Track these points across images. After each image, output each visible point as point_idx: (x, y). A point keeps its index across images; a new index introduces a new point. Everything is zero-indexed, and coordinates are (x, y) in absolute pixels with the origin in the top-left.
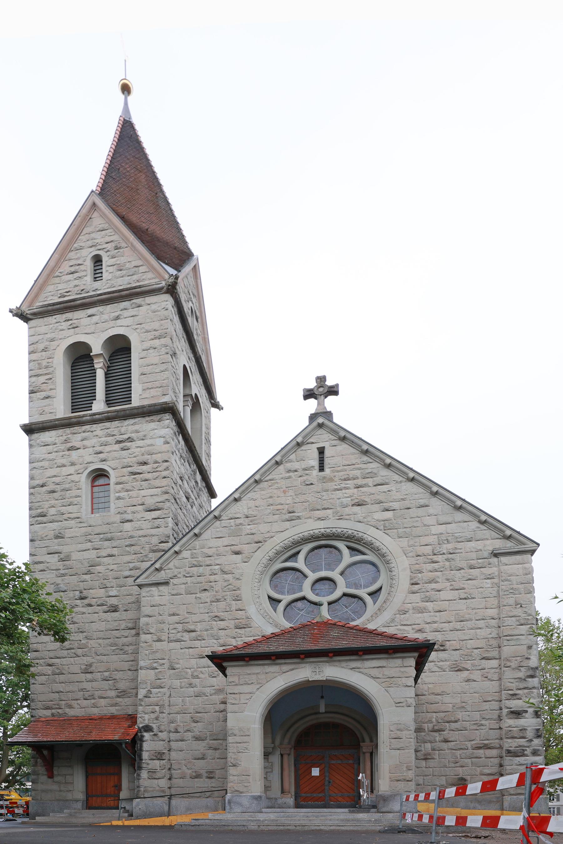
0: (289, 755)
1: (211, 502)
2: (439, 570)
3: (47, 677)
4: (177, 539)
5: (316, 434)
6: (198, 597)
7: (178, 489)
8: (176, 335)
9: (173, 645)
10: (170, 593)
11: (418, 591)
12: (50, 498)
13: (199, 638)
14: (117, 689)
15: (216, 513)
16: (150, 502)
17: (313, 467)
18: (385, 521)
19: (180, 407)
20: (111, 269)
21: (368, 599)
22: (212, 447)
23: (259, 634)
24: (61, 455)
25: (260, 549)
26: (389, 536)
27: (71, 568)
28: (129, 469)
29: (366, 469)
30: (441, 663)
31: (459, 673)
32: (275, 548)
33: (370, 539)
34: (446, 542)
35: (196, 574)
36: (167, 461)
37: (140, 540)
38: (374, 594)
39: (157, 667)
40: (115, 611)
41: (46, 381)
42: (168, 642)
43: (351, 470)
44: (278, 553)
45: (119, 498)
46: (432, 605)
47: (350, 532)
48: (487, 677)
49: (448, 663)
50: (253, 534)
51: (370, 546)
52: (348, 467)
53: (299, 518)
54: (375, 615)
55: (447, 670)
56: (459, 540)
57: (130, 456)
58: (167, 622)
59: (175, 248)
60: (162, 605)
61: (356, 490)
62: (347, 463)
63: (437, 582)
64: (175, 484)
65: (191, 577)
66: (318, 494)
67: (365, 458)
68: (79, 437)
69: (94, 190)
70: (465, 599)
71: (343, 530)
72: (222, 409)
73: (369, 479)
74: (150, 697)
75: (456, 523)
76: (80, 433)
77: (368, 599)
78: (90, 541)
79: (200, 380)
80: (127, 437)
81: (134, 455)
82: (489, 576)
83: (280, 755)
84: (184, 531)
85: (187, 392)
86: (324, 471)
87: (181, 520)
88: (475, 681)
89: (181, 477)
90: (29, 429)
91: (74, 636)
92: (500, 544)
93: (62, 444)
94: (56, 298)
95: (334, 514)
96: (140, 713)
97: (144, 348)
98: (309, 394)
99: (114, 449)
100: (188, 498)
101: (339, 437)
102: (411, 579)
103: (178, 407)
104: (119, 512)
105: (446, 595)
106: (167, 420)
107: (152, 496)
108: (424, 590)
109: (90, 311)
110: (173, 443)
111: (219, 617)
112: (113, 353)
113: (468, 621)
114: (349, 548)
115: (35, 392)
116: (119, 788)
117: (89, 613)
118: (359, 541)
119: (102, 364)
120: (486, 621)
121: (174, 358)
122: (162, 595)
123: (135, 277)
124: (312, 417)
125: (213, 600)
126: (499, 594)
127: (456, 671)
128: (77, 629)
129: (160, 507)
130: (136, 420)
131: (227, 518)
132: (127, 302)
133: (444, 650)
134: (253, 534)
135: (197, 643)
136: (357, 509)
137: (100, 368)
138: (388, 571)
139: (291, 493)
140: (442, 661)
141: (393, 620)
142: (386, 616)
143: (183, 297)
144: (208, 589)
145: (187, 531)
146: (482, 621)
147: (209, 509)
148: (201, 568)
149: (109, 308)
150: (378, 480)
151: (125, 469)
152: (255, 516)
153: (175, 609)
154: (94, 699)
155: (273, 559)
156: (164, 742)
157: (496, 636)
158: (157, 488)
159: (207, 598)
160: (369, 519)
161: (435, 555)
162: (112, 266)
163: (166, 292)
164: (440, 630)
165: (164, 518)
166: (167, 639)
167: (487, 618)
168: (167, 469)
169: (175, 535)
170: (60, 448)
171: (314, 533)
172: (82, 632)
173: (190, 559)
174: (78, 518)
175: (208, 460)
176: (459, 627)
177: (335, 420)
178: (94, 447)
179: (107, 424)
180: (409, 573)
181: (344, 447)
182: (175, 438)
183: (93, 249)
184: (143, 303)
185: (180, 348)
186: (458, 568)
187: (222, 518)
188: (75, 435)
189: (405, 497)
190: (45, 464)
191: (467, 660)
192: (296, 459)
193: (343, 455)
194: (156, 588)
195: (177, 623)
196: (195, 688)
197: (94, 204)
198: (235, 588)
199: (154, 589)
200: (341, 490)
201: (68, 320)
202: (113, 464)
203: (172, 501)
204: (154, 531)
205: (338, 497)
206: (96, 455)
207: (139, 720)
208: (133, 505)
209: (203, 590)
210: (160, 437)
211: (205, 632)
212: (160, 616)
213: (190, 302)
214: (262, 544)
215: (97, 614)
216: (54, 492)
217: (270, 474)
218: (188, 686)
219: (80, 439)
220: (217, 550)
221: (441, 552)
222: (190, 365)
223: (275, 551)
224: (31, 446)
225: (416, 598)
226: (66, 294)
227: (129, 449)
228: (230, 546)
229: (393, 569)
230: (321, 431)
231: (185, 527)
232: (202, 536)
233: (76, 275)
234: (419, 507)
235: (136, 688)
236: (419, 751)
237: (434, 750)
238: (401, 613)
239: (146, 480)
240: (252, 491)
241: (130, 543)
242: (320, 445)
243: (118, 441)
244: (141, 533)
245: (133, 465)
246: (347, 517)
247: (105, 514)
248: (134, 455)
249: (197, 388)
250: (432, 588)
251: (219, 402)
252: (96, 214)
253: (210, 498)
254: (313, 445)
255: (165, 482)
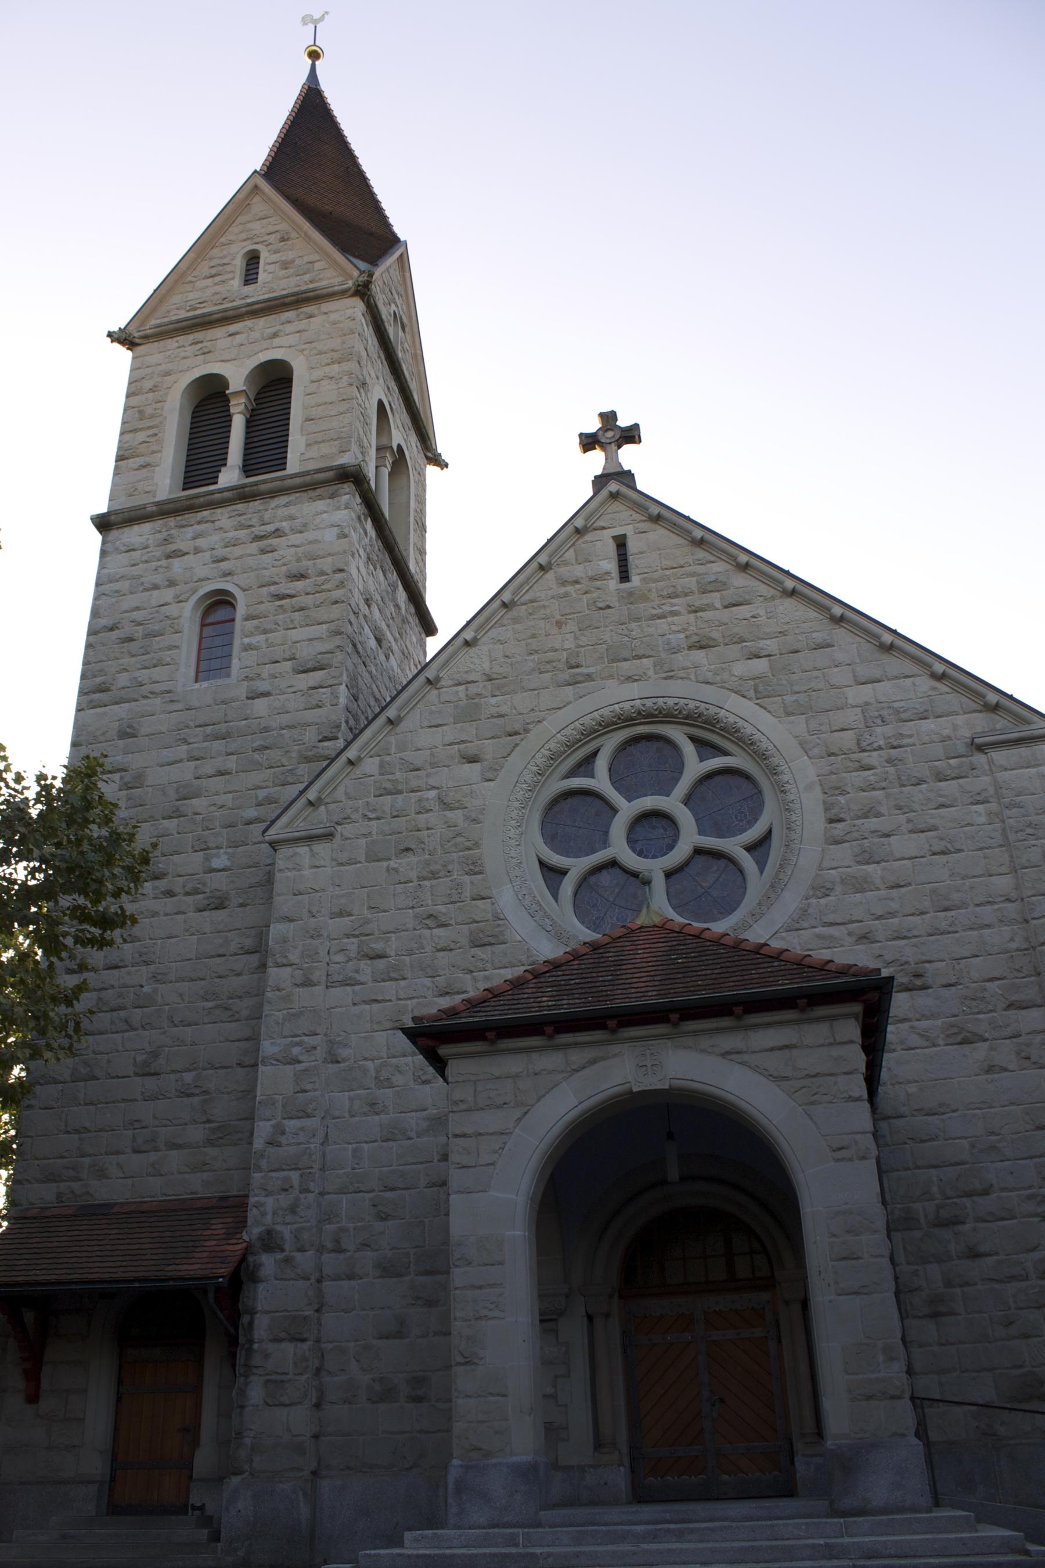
0: (607, 1316)
1: (425, 643)
2: (877, 786)
3: (60, 1086)
4: (354, 731)
5: (609, 511)
6: (393, 869)
7: (361, 625)
8: (368, 355)
9: (336, 992)
10: (335, 860)
11: (846, 838)
12: (122, 652)
13: (393, 975)
14: (209, 1121)
15: (430, 673)
16: (307, 652)
17: (608, 573)
18: (754, 679)
19: (371, 472)
20: (271, 268)
21: (747, 861)
22: (428, 535)
23: (523, 958)
24: (153, 568)
25: (518, 749)
26: (769, 712)
27: (141, 805)
28: (272, 588)
29: (705, 574)
30: (924, 1024)
31: (966, 1049)
32: (547, 747)
33: (732, 719)
34: (879, 721)
35: (388, 810)
36: (341, 570)
37: (282, 735)
38: (759, 847)
39: (301, 1058)
40: (220, 906)
41: (148, 440)
42: (327, 987)
43: (679, 578)
44: (553, 757)
45: (248, 648)
46: (879, 872)
47: (692, 705)
48: (1028, 1058)
49: (939, 1022)
50: (502, 716)
51: (732, 733)
52: (671, 571)
53: (589, 677)
54: (768, 900)
55: (941, 1042)
56: (904, 716)
57: (277, 563)
58: (325, 935)
59: (372, 234)
60: (317, 891)
61: (692, 616)
62: (670, 564)
63: (878, 815)
64: (354, 613)
65: (378, 819)
66: (623, 627)
67: (701, 554)
68: (190, 532)
69: (258, 170)
70: (943, 853)
71: (677, 700)
72: (447, 466)
73: (713, 594)
74: (280, 1145)
75: (889, 680)
76: (192, 525)
77: (747, 861)
78: (185, 741)
79: (408, 421)
80: (273, 530)
81: (284, 560)
82: (978, 798)
83: (585, 1319)
84: (369, 711)
85: (384, 441)
86: (628, 581)
87: (364, 687)
88: (1006, 1070)
89: (368, 600)
90: (103, 523)
91: (129, 973)
92: (979, 723)
93: (158, 546)
94: (183, 312)
95: (658, 668)
96: (256, 1191)
97: (314, 378)
98: (589, 442)
99: (249, 552)
100: (379, 641)
101: (649, 515)
102: (826, 810)
103: (365, 472)
104: (247, 677)
105: (903, 844)
106: (346, 494)
107: (311, 640)
108: (856, 835)
109: (233, 328)
110: (354, 536)
111: (436, 917)
112: (263, 388)
113: (958, 909)
114: (693, 739)
115: (127, 458)
116: (192, 1432)
117: (166, 915)
118: (711, 723)
119: (243, 406)
120: (996, 907)
121: (362, 391)
122: (317, 864)
123: (307, 277)
124: (600, 482)
125: (425, 874)
126: (1007, 838)
127: (960, 1043)
128: (137, 956)
129: (325, 662)
130: (292, 497)
131: (450, 683)
132: (291, 312)
133: (924, 987)
134: (502, 716)
135: (390, 989)
136: (699, 655)
137: (238, 413)
138: (778, 792)
139: (572, 626)
140: (924, 1017)
141: (804, 913)
142: (790, 902)
143: (380, 300)
144: (413, 847)
145: (377, 710)
146: (988, 908)
147: (422, 659)
148: (400, 797)
149: (262, 322)
150: (729, 595)
151: (265, 589)
152: (505, 677)
153: (343, 901)
154: (156, 1150)
155: (546, 771)
156: (308, 1283)
157: (1025, 946)
158: (320, 624)
159: (412, 869)
160: (725, 676)
161: (864, 751)
162: (273, 263)
163: (353, 295)
164: (907, 934)
165: (331, 686)
166: (324, 978)
167: (997, 900)
168: (341, 585)
169: (352, 722)
170: (153, 554)
171: (621, 709)
172: (147, 963)
173: (377, 777)
174: (168, 692)
175: (420, 561)
176: (944, 925)
177: (639, 487)
178: (214, 549)
179: (241, 507)
180: (821, 796)
181: (659, 534)
182: (358, 525)
183: (248, 242)
184: (316, 312)
185: (373, 375)
186: (914, 781)
187: (443, 683)
188: (183, 530)
189: (786, 627)
190: (124, 586)
191: (978, 1013)
192: (576, 560)
193: (659, 549)
194: (306, 848)
195: (348, 936)
196: (383, 1116)
197: (256, 187)
198: (468, 844)
199: (303, 850)
200: (665, 617)
201: (198, 343)
202: (241, 579)
203: (348, 650)
204: (311, 715)
205: (660, 632)
206: (214, 565)
207: (252, 1214)
208: (274, 660)
209: (403, 851)
210: (332, 526)
211: (407, 958)
212: (313, 919)
213: (393, 305)
214: (522, 736)
215: (183, 916)
216: (130, 639)
217: (531, 591)
218: (366, 1109)
219: (190, 535)
220: (432, 754)
221: (876, 745)
222: (391, 399)
223: (547, 753)
224: (103, 553)
225: (843, 854)
226: (198, 306)
227: (276, 550)
228: (458, 743)
229: (788, 787)
230: (616, 506)
231: (372, 703)
232: (402, 725)
233: (217, 279)
234: (815, 649)
235: (251, 1118)
236: (916, 1290)
237: (949, 1284)
238: (820, 894)
239: (302, 609)
240: (497, 625)
241: (263, 743)
242: (618, 531)
243: (256, 536)
244: (285, 719)
245: (281, 580)
246: (682, 674)
247: (220, 682)
248: (284, 560)
249: (401, 435)
250: (873, 829)
251: (440, 455)
252: (257, 199)
253: (423, 635)
254: (605, 531)
255: (335, 612)
